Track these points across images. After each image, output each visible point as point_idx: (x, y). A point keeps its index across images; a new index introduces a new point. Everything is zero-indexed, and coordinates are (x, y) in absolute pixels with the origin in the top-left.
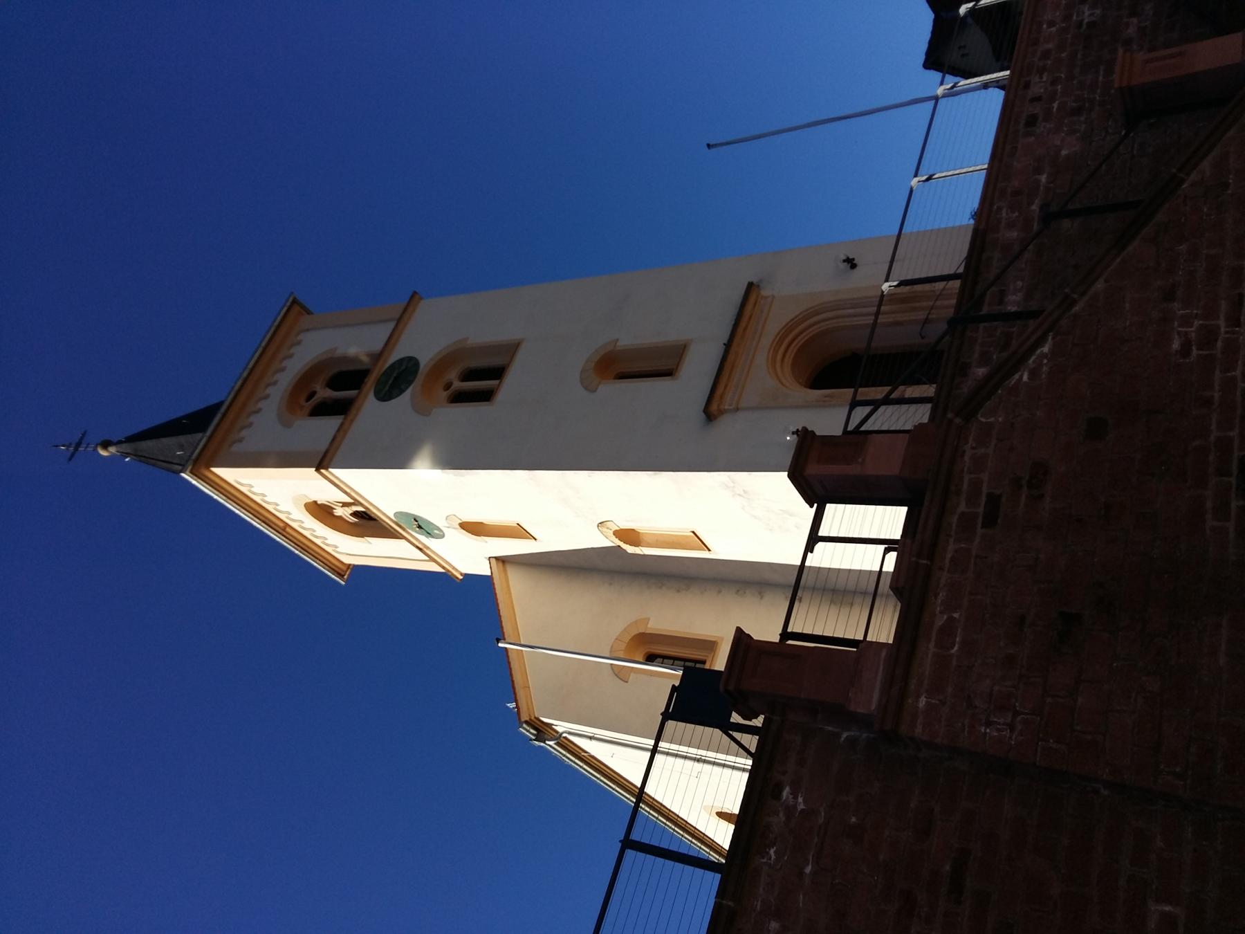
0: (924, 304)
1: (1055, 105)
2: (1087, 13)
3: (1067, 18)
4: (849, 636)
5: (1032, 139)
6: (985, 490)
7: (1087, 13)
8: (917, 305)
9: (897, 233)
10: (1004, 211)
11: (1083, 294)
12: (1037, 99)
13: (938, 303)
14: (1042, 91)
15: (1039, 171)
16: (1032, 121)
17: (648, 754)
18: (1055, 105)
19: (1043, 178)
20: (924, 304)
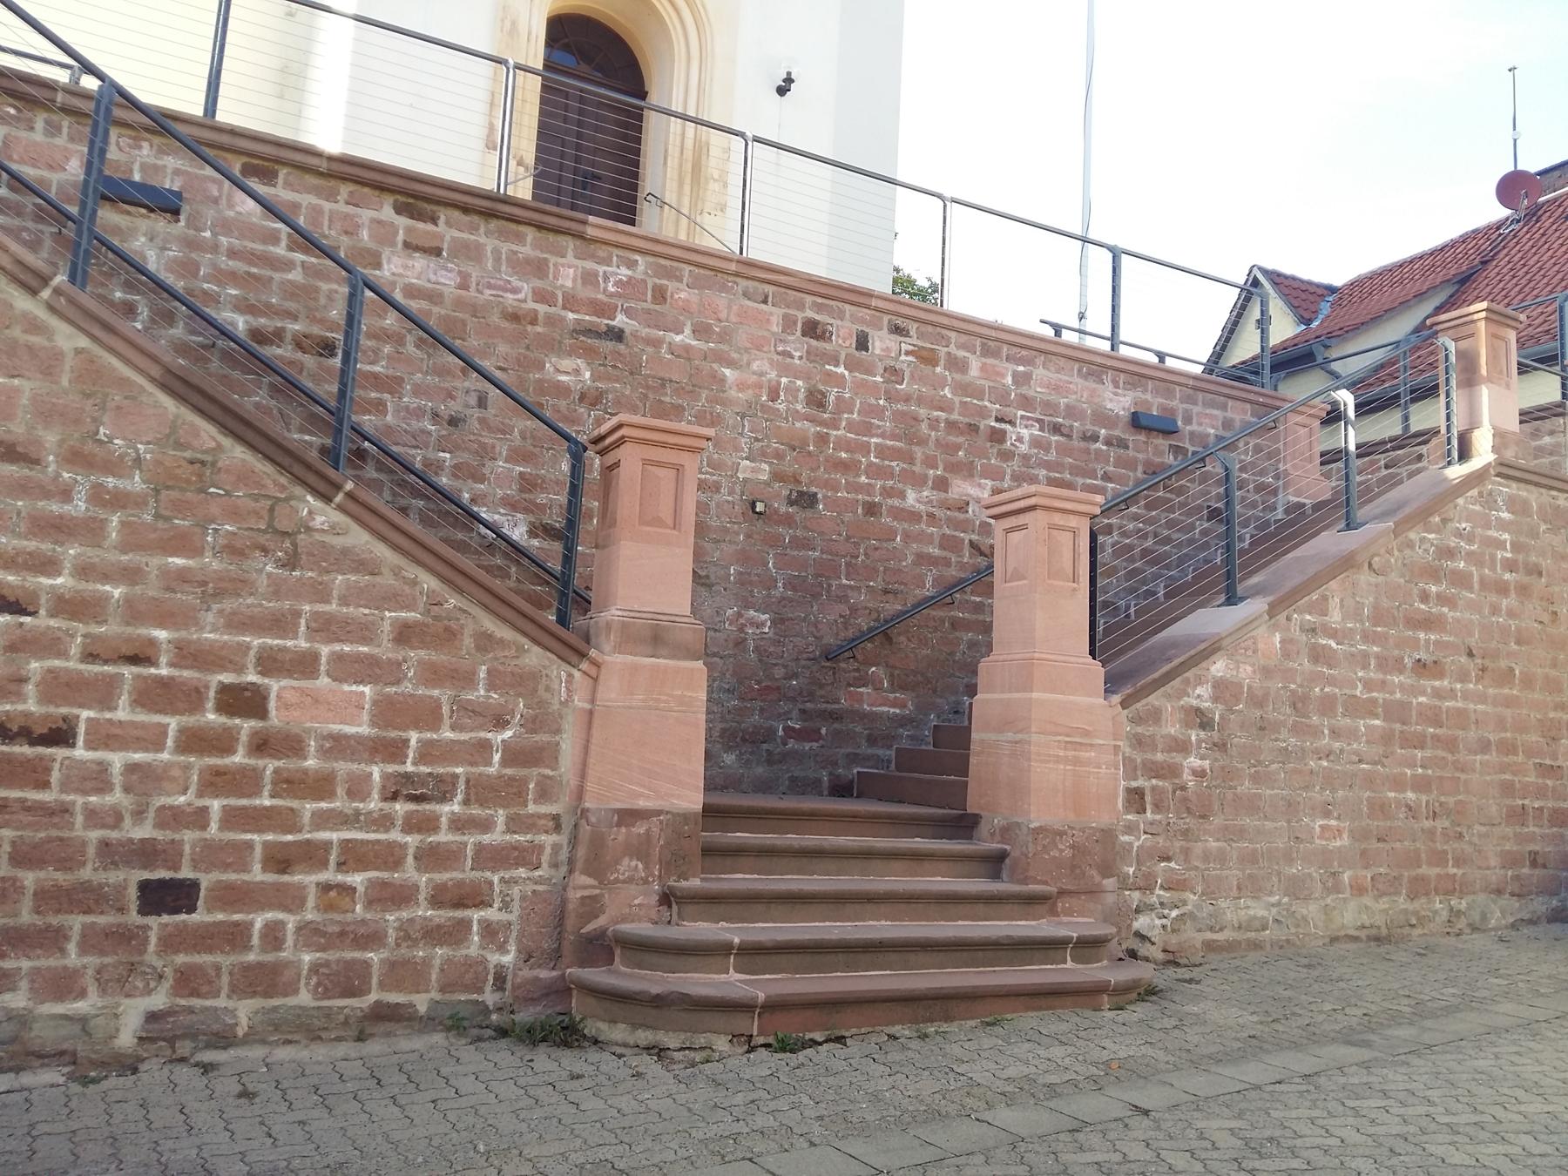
0: (686, 201)
1: (841, 370)
2: (1025, 433)
3: (1026, 402)
4: (222, 103)
5: (776, 328)
6: (277, 276)
7: (1025, 433)
8: (687, 188)
9: (900, 178)
10: (624, 272)
11: (51, 308)
12: (862, 343)
13: (684, 221)
14: (877, 352)
15: (701, 331)
16: (813, 330)
17: (1078, 232)
18: (841, 370)
19: (684, 338)
20: (686, 201)
